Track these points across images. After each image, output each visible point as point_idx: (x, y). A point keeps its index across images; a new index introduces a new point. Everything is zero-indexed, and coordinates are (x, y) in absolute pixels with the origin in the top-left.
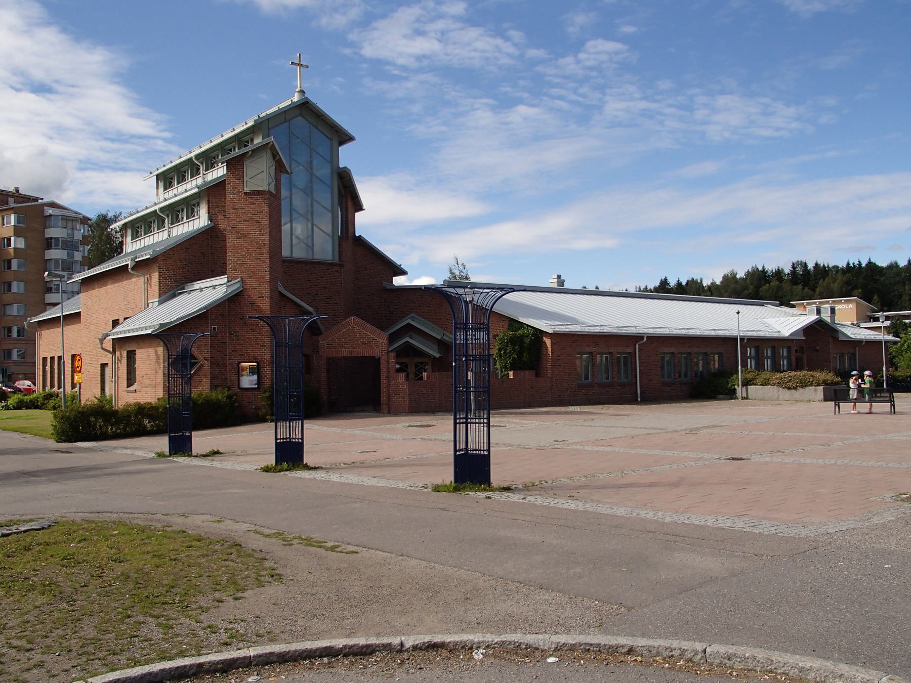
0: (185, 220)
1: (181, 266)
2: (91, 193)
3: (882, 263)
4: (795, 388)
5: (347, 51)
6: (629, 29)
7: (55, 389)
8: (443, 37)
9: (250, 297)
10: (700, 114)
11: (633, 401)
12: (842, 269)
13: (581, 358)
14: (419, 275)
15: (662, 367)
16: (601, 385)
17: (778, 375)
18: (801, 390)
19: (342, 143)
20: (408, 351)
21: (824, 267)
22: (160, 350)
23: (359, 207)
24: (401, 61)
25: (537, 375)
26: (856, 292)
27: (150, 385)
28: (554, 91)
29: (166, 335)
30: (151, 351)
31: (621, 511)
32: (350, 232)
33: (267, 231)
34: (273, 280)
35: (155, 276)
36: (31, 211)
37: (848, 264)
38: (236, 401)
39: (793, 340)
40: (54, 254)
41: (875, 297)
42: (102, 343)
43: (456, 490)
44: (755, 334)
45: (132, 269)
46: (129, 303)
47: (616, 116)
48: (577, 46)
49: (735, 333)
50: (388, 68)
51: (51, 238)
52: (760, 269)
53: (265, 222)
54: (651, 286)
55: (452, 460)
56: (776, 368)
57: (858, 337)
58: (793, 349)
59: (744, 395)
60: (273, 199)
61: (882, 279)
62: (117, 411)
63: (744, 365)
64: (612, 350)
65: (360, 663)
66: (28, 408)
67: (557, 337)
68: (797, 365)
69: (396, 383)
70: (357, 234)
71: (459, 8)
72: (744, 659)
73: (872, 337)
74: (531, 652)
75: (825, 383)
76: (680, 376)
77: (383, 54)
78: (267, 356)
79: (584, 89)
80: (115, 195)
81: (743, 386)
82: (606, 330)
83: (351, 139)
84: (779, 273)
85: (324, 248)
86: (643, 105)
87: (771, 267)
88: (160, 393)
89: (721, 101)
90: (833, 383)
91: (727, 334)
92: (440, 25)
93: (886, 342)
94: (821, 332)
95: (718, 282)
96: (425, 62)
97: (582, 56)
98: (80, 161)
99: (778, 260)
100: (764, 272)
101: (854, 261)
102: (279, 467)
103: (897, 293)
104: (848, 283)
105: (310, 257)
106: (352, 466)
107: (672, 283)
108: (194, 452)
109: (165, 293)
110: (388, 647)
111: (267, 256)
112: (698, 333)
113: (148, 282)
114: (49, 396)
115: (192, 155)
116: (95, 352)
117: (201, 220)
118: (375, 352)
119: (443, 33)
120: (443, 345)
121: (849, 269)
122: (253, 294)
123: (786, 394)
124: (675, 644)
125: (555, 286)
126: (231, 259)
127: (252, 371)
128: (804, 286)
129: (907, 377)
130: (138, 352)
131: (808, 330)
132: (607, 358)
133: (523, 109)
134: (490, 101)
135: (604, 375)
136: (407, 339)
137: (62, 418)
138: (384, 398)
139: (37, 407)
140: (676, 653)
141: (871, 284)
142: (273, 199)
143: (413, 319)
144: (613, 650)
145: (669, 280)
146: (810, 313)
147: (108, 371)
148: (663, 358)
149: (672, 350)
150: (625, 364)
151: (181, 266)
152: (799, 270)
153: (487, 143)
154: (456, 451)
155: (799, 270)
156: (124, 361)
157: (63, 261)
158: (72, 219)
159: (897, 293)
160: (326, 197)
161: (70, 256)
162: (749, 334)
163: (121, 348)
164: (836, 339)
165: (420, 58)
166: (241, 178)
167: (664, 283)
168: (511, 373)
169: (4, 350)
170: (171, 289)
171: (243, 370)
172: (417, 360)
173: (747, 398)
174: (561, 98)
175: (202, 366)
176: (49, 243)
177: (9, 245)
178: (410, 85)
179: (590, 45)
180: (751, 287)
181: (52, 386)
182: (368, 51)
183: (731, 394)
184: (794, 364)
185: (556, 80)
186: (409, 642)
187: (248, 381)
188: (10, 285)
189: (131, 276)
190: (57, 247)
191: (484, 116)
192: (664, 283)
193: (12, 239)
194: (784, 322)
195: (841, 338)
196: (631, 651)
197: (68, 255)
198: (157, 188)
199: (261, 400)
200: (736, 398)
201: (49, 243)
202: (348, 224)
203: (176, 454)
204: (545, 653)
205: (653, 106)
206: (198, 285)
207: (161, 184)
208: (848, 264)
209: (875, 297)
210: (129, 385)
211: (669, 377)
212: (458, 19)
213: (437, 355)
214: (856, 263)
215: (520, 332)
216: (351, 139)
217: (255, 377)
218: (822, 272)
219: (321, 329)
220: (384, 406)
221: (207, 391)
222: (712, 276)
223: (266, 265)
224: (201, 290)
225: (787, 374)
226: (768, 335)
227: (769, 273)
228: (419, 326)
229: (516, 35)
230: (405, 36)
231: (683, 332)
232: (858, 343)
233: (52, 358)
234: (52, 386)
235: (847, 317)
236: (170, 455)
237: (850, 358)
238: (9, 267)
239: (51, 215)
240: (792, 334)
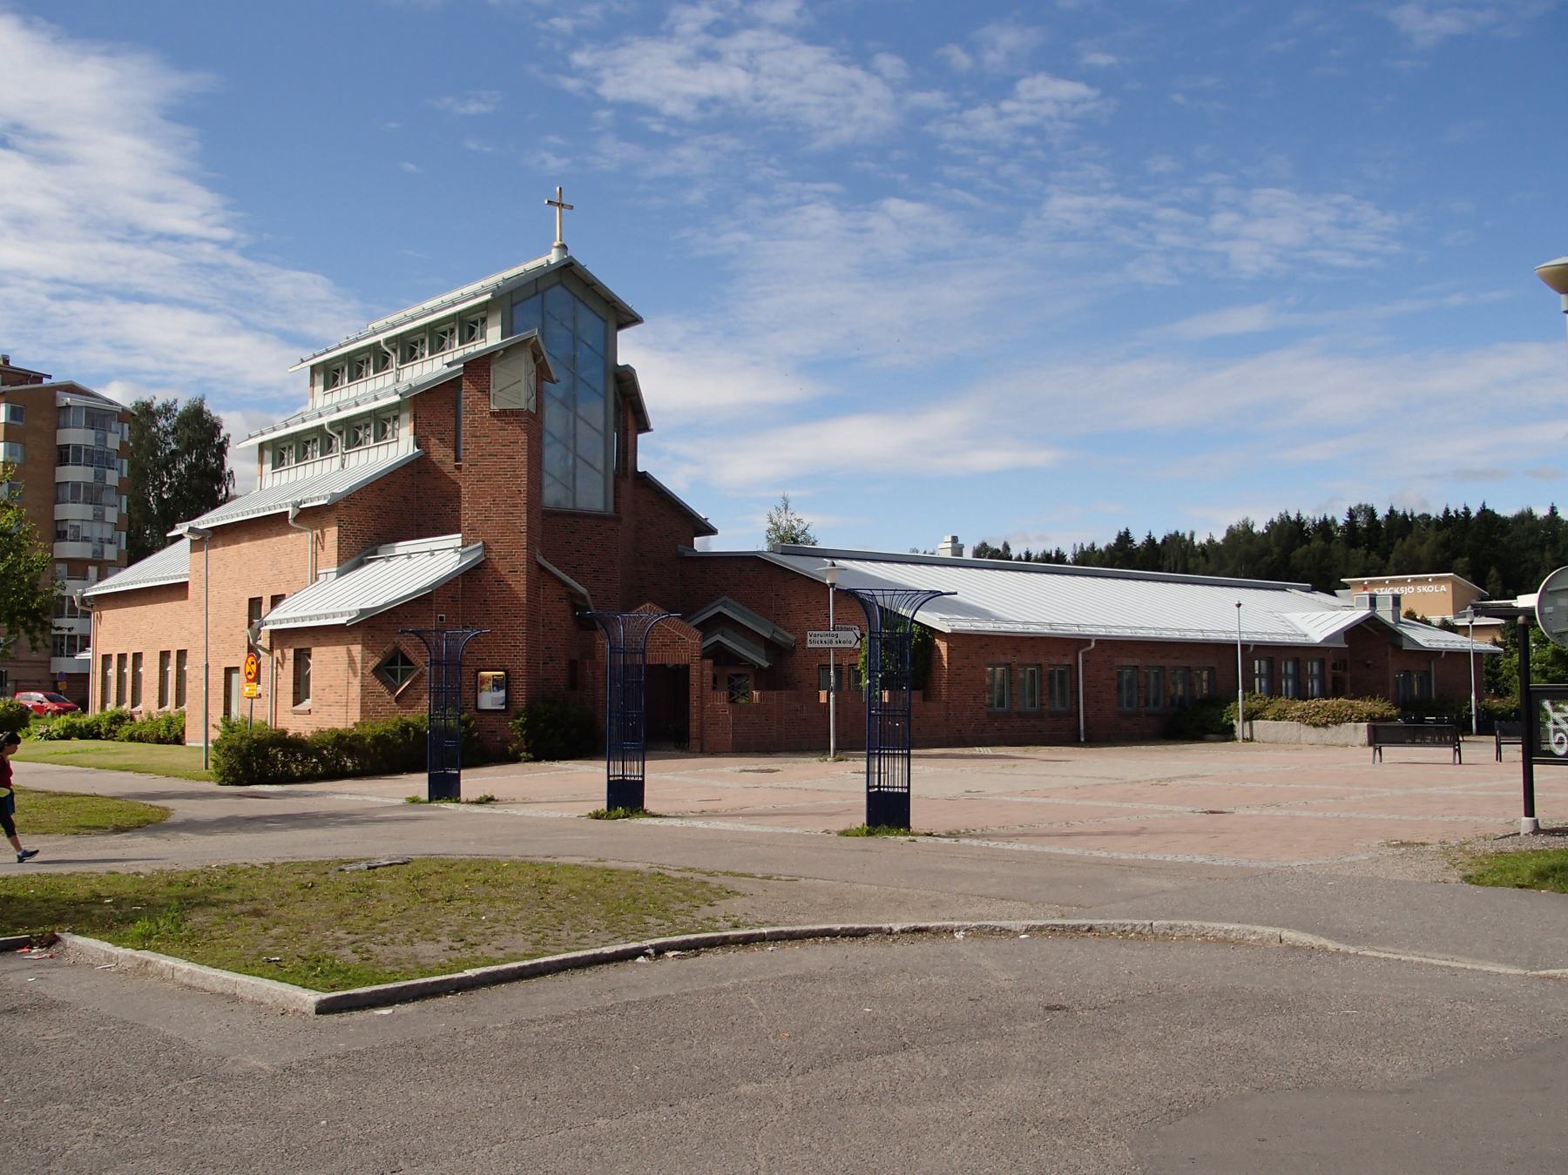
1: (377, 518)
2: (77, 343)
3: (1506, 509)
4: (1325, 725)
5: (571, 84)
6: (1101, 60)
7: (127, 706)
8: (751, 68)
9: (496, 571)
10: (1223, 221)
11: (1072, 740)
12: (1437, 520)
13: (993, 673)
14: (736, 532)
15: (1119, 689)
16: (1023, 715)
17: (1300, 704)
18: (1334, 728)
19: (621, 326)
20: (719, 655)
21: (1405, 516)
22: (357, 649)
23: (644, 427)
24: (672, 107)
25: (926, 698)
26: (1461, 562)
27: (337, 699)
28: (952, 172)
29: (372, 626)
30: (341, 650)
31: (1071, 852)
32: (630, 467)
33: (524, 471)
34: (530, 546)
35: (332, 534)
36: (37, 401)
37: (1447, 511)
38: (474, 729)
39: (1328, 649)
41: (1493, 572)
43: (869, 833)
44: (1267, 638)
45: (295, 520)
47: (1068, 222)
48: (999, 88)
49: (1235, 637)
50: (645, 119)
51: (67, 446)
52: (1293, 517)
53: (522, 458)
54: (1101, 545)
55: (864, 801)
56: (1301, 694)
57: (1435, 645)
58: (1329, 664)
59: (1247, 735)
60: (532, 421)
61: (1505, 539)
63: (1249, 687)
64: (1042, 660)
65: (860, 941)
66: (81, 738)
67: (955, 638)
68: (1334, 687)
69: (710, 704)
70: (640, 470)
71: (784, 11)
72: (1183, 928)
73: (1458, 646)
74: (1005, 931)
75: (1370, 717)
76: (1147, 703)
77: (637, 91)
79: (1011, 169)
80: (126, 348)
81: (1245, 720)
82: (1033, 629)
84: (1325, 526)
85: (593, 495)
86: (1116, 202)
87: (1311, 514)
88: (355, 715)
89: (1263, 197)
90: (1383, 719)
91: (1223, 637)
92: (747, 39)
93: (1478, 654)
94: (1370, 636)
95: (1219, 538)
96: (716, 111)
97: (1007, 106)
98: (57, 281)
99: (1326, 501)
100: (1299, 523)
101: (1456, 507)
102: (613, 814)
103: (1530, 565)
104: (1445, 545)
105: (570, 506)
106: (702, 814)
107: (1139, 539)
108: (463, 797)
109: (347, 558)
110: (879, 930)
111: (524, 509)
112: (1176, 635)
113: (319, 541)
114: (119, 719)
117: (401, 446)
118: (682, 658)
119: (752, 53)
120: (771, 647)
121: (1448, 521)
122: (502, 567)
123: (1310, 734)
124: (1128, 921)
125: (947, 554)
126: (467, 513)
127: (497, 684)
128: (1369, 550)
129: (1511, 711)
130: (314, 651)
131: (1353, 633)
132: (1032, 673)
133: (894, 205)
134: (832, 187)
135: (1028, 701)
136: (718, 637)
137: (229, 748)
138: (694, 728)
139: (97, 736)
140: (1128, 928)
141: (1488, 551)
142: (532, 421)
143: (725, 605)
144: (1076, 929)
145: (1133, 535)
146: (1360, 604)
148: (1120, 674)
149: (1137, 662)
150: (1062, 683)
151: (377, 518)
152: (1361, 520)
153: (811, 260)
154: (869, 787)
155: (1361, 520)
156: (289, 665)
157: (88, 486)
158: (101, 416)
159: (1530, 565)
160: (596, 411)
161: (100, 477)
162: (1257, 638)
163: (282, 647)
164: (1398, 648)
165: (704, 104)
166: (485, 391)
167: (1125, 538)
168: (886, 694)
170: (355, 555)
171: (482, 683)
172: (732, 671)
173: (1251, 740)
174: (967, 186)
176: (63, 455)
178: (684, 152)
179: (1023, 85)
180: (1277, 550)
181: (120, 702)
182: (611, 90)
183: (1227, 734)
184: (1329, 686)
185: (962, 151)
186: (897, 927)
187: (490, 699)
189: (289, 530)
190: (77, 462)
191: (822, 218)
192: (1125, 538)
194: (1311, 618)
195: (1406, 646)
196: (1090, 929)
197: (104, 477)
198: (312, 385)
199: (515, 725)
200: (1235, 739)
201: (63, 455)
202: (627, 452)
203: (438, 798)
204: (1016, 934)
205: (1133, 205)
206: (402, 547)
207: (320, 379)
208: (1447, 511)
209: (1493, 572)
210: (297, 702)
211: (1130, 704)
212: (784, 29)
213: (765, 664)
214: (1461, 510)
215: (900, 630)
217: (502, 693)
218: (1400, 524)
219: (609, 622)
220: (693, 742)
222: (1209, 528)
223: (522, 522)
224: (409, 556)
225: (1313, 703)
226: (1287, 640)
227: (1309, 525)
228: (750, 625)
229: (889, 63)
230: (680, 62)
231: (1152, 634)
232: (1435, 654)
233: (122, 657)
234: (120, 702)
235: (1430, 611)
236: (430, 800)
237: (1421, 680)
239: (68, 407)
240: (1326, 640)
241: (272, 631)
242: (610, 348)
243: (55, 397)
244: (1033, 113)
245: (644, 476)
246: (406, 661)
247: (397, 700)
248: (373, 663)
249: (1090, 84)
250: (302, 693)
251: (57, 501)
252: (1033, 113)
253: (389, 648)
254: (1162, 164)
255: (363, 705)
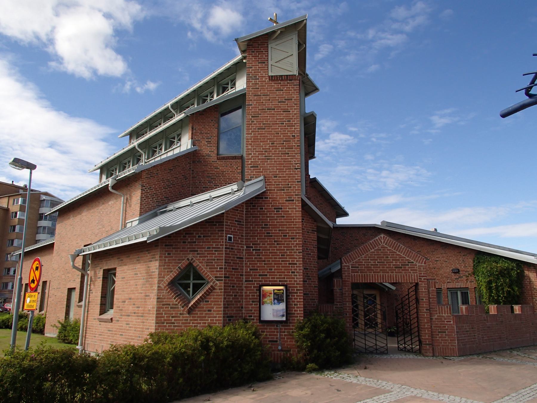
0: (163, 152)
6: (353, 129)
10: (385, 173)
19: (307, 94)
22: (155, 266)
29: (168, 243)
40: (43, 223)
42: (74, 260)
46: (103, 227)
62: (94, 361)
78: (298, 278)
83: (316, 89)
86: (356, 168)
97: (327, 141)
98: (63, 185)
109: (146, 212)
115: (169, 104)
116: (63, 277)
122: (280, 198)
127: (278, 298)
147: (75, 296)
156: (99, 283)
157: (49, 228)
169: (4, 283)
171: (265, 296)
175: (212, 288)
176: (41, 217)
177: (16, 216)
179: (331, 136)
188: (13, 241)
193: (18, 213)
201: (41, 217)
210: (103, 311)
216: (316, 89)
221: (218, 325)
234: (404, 248)
238: (14, 230)
239: (44, 200)
241: (83, 255)
242: (302, 105)
243: (40, 196)
244: (334, 143)
245: (315, 180)
246: (198, 276)
247: (190, 311)
248: (168, 278)
249: (350, 135)
250: (108, 305)
251: (37, 233)
252: (334, 143)
253: (185, 263)
254: (369, 157)
255: (159, 316)
